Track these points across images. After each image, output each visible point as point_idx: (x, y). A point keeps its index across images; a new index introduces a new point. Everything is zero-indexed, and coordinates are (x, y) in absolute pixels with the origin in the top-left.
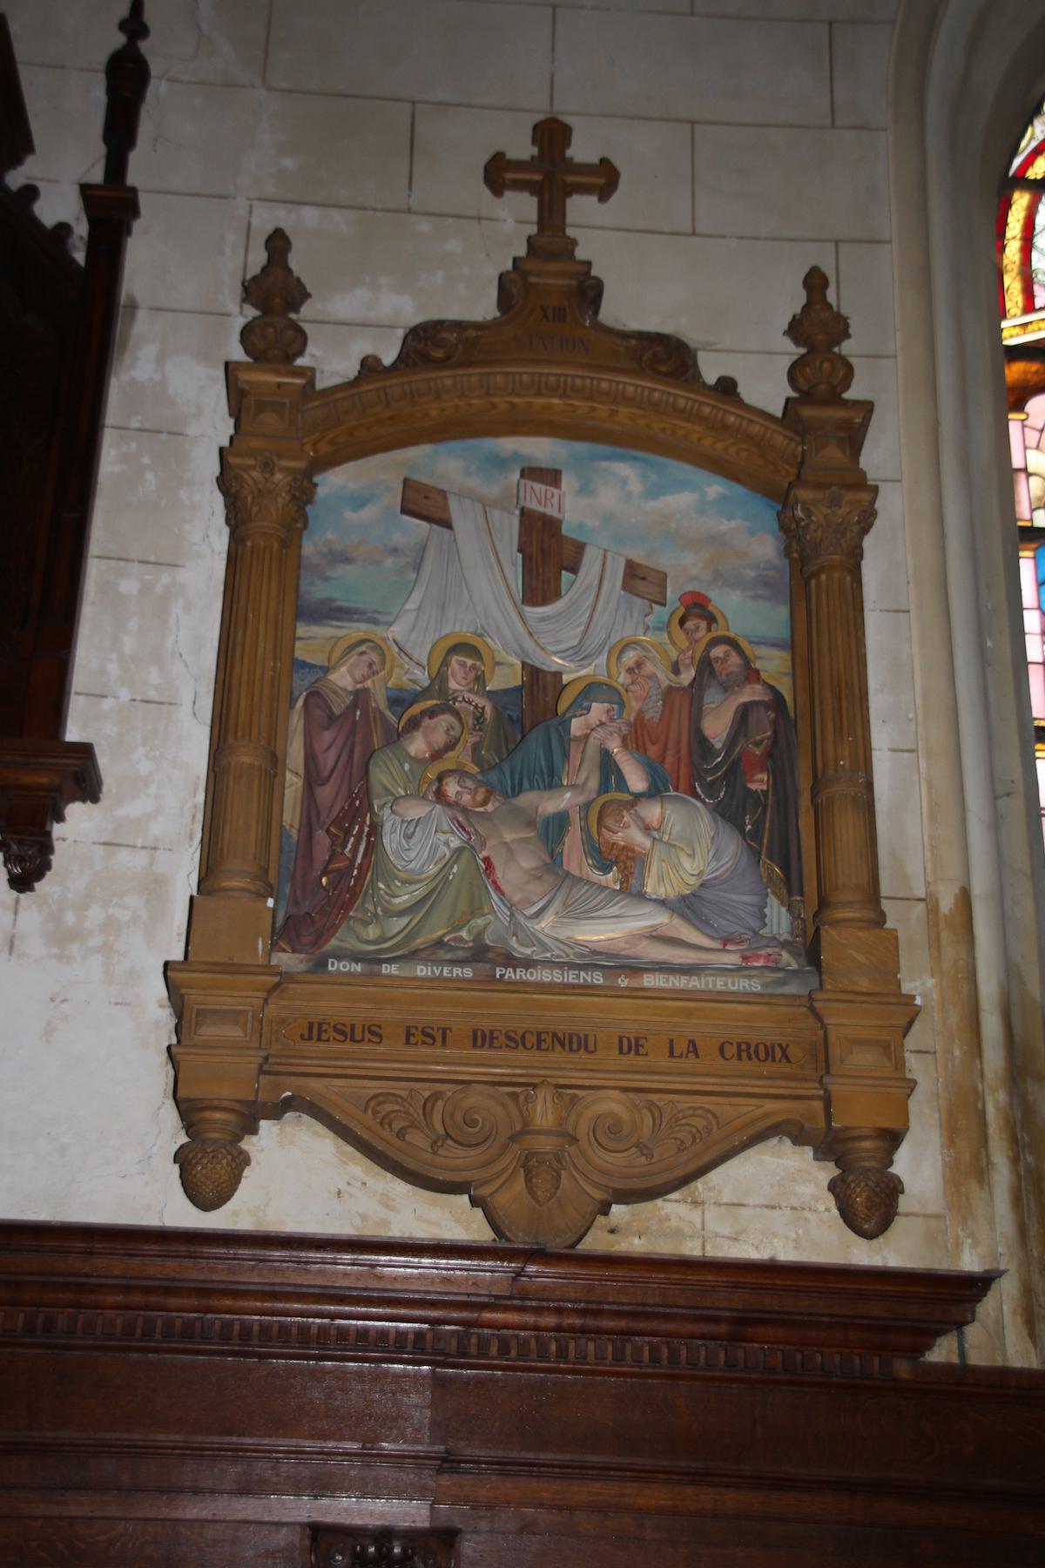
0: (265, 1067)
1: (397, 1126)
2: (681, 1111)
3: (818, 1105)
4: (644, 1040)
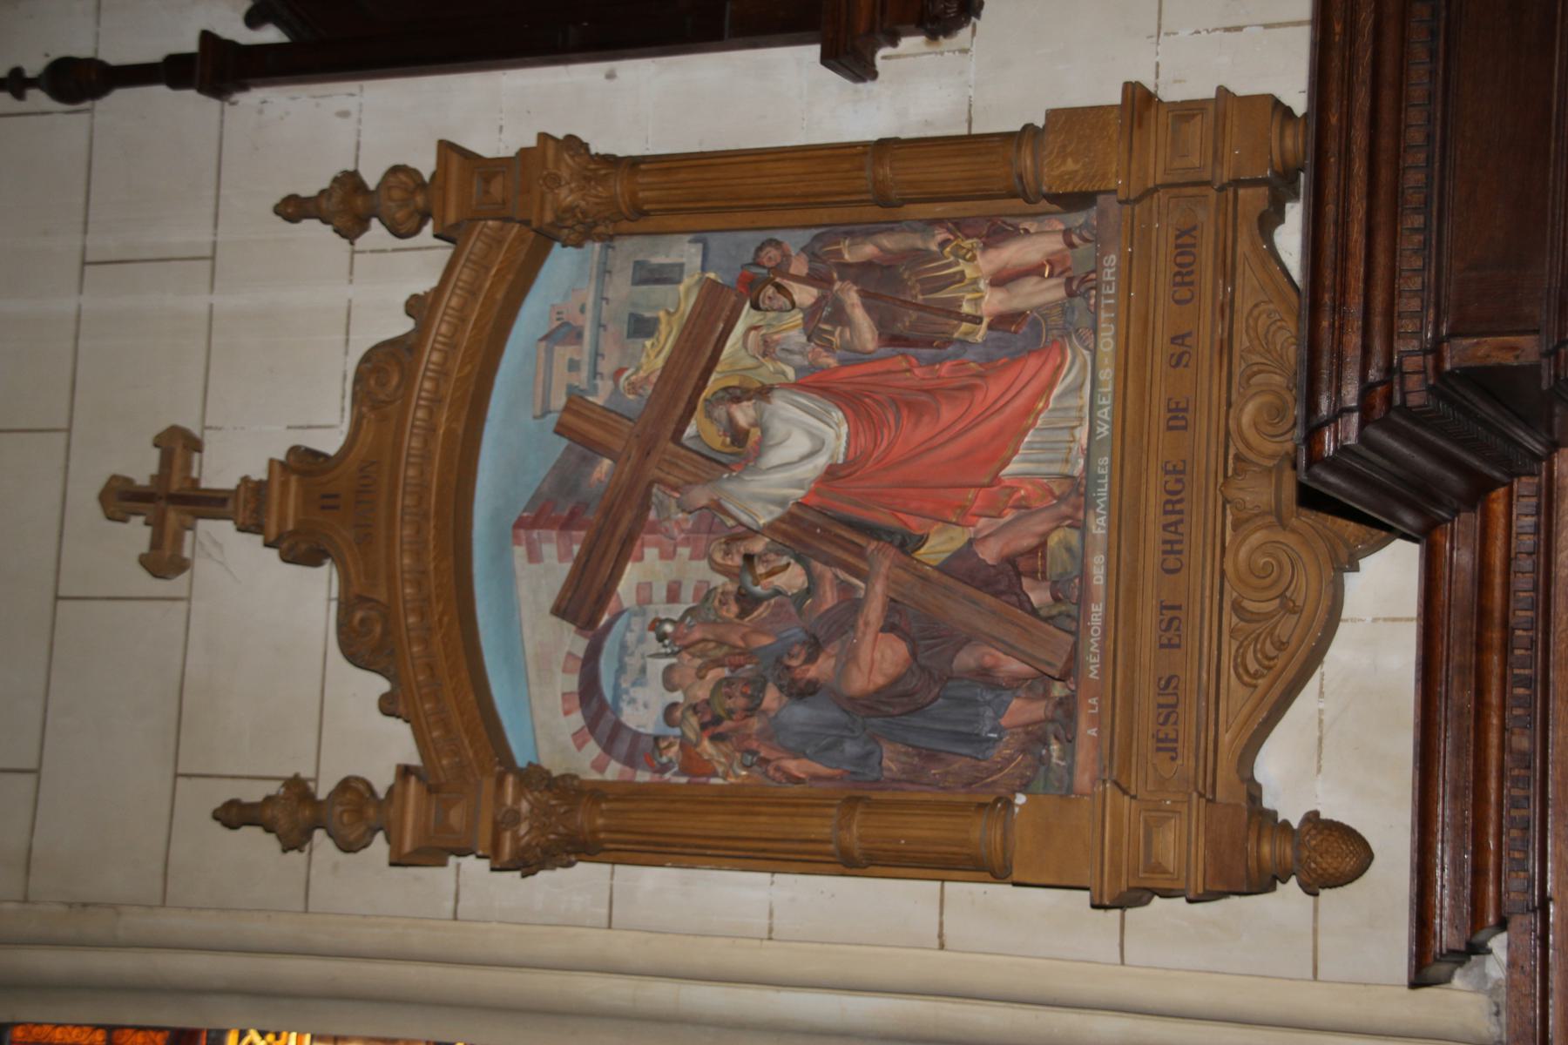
1: (1271, 651)
2: (1250, 341)
4: (1163, 638)
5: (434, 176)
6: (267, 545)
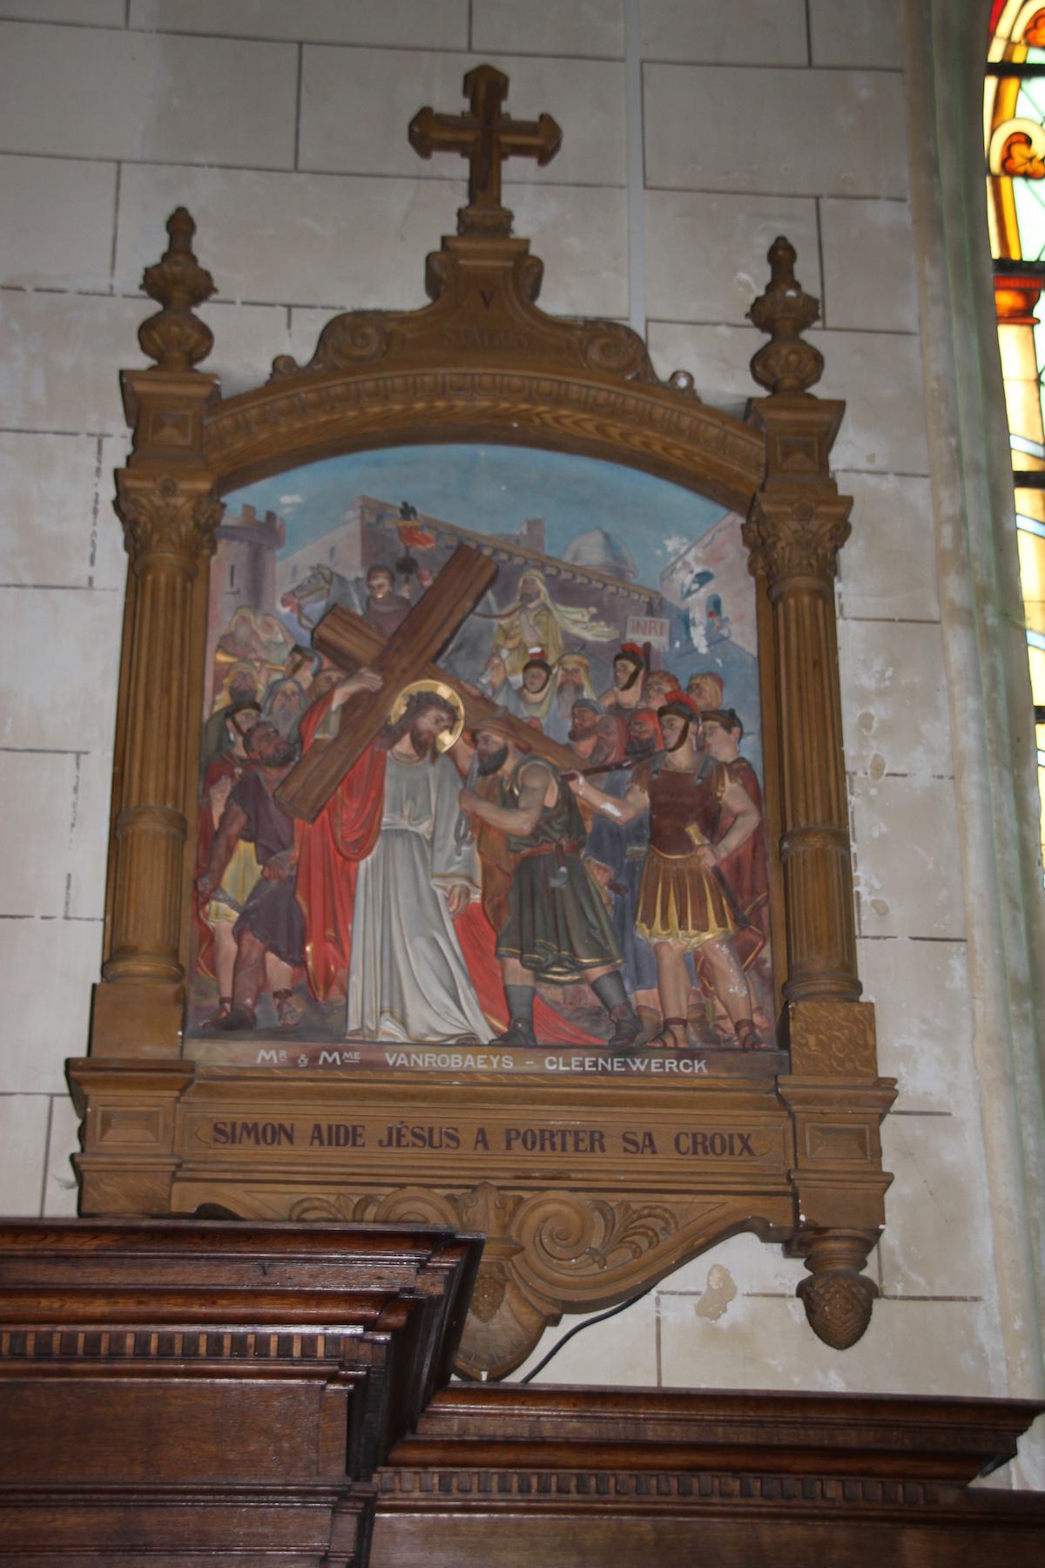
0: (180, 1174)
2: (634, 1212)
5: (811, 397)
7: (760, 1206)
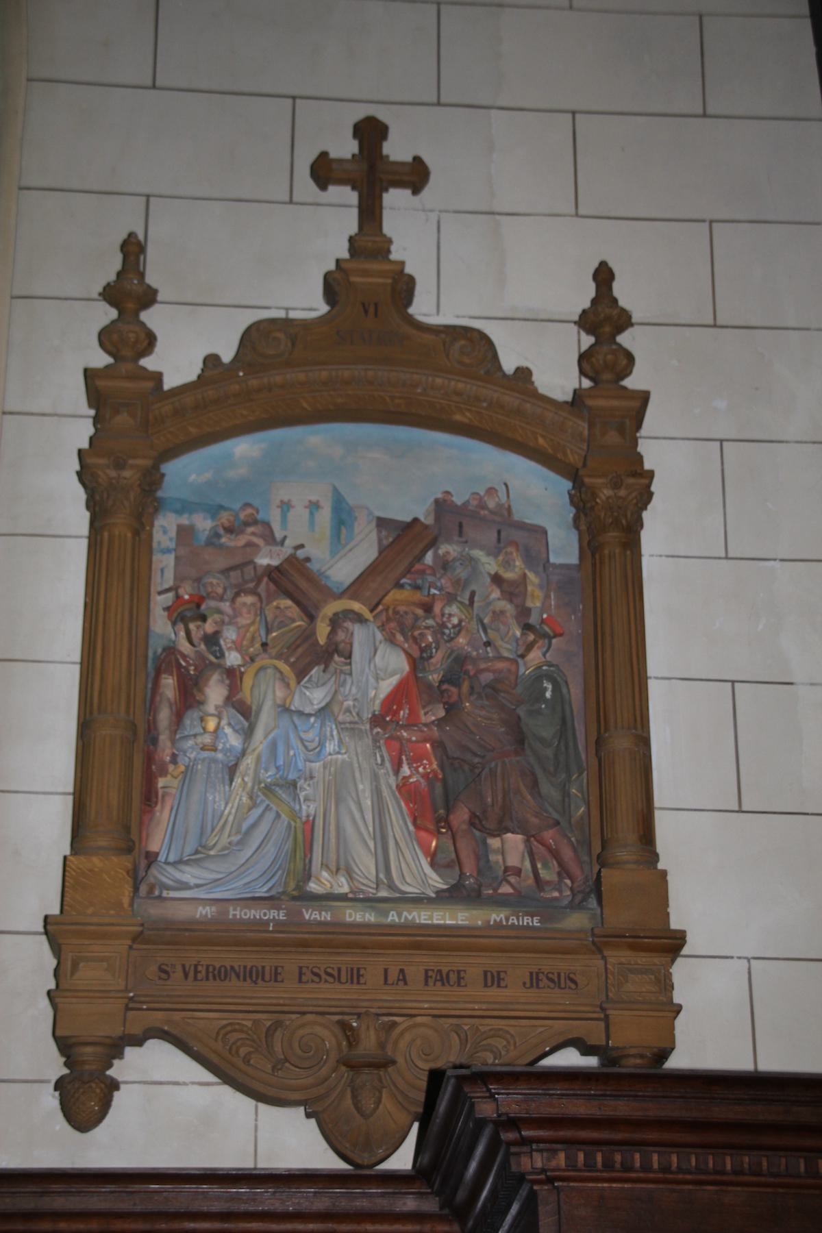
0: (131, 1005)
1: (243, 1051)
2: (485, 1032)
3: (602, 1024)
5: (625, 388)
6: (338, 262)
7: (578, 1029)
